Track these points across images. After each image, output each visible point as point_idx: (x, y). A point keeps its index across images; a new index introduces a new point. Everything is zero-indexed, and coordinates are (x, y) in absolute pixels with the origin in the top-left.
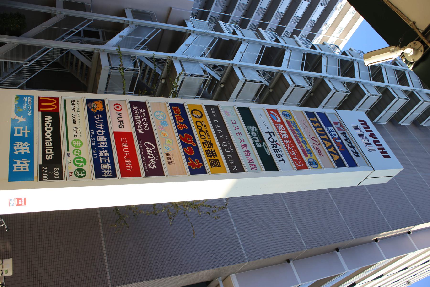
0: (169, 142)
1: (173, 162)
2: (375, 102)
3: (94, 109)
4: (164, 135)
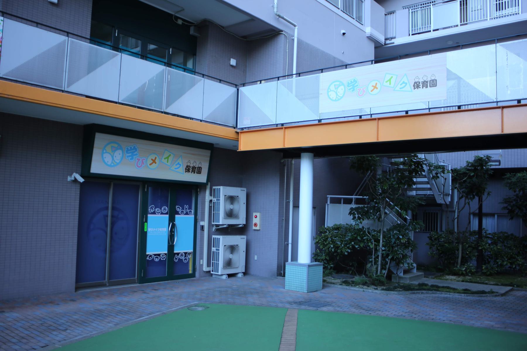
0: (390, 80)
1: (433, 78)
2: (346, 283)
3: (373, 218)
4: (375, 87)
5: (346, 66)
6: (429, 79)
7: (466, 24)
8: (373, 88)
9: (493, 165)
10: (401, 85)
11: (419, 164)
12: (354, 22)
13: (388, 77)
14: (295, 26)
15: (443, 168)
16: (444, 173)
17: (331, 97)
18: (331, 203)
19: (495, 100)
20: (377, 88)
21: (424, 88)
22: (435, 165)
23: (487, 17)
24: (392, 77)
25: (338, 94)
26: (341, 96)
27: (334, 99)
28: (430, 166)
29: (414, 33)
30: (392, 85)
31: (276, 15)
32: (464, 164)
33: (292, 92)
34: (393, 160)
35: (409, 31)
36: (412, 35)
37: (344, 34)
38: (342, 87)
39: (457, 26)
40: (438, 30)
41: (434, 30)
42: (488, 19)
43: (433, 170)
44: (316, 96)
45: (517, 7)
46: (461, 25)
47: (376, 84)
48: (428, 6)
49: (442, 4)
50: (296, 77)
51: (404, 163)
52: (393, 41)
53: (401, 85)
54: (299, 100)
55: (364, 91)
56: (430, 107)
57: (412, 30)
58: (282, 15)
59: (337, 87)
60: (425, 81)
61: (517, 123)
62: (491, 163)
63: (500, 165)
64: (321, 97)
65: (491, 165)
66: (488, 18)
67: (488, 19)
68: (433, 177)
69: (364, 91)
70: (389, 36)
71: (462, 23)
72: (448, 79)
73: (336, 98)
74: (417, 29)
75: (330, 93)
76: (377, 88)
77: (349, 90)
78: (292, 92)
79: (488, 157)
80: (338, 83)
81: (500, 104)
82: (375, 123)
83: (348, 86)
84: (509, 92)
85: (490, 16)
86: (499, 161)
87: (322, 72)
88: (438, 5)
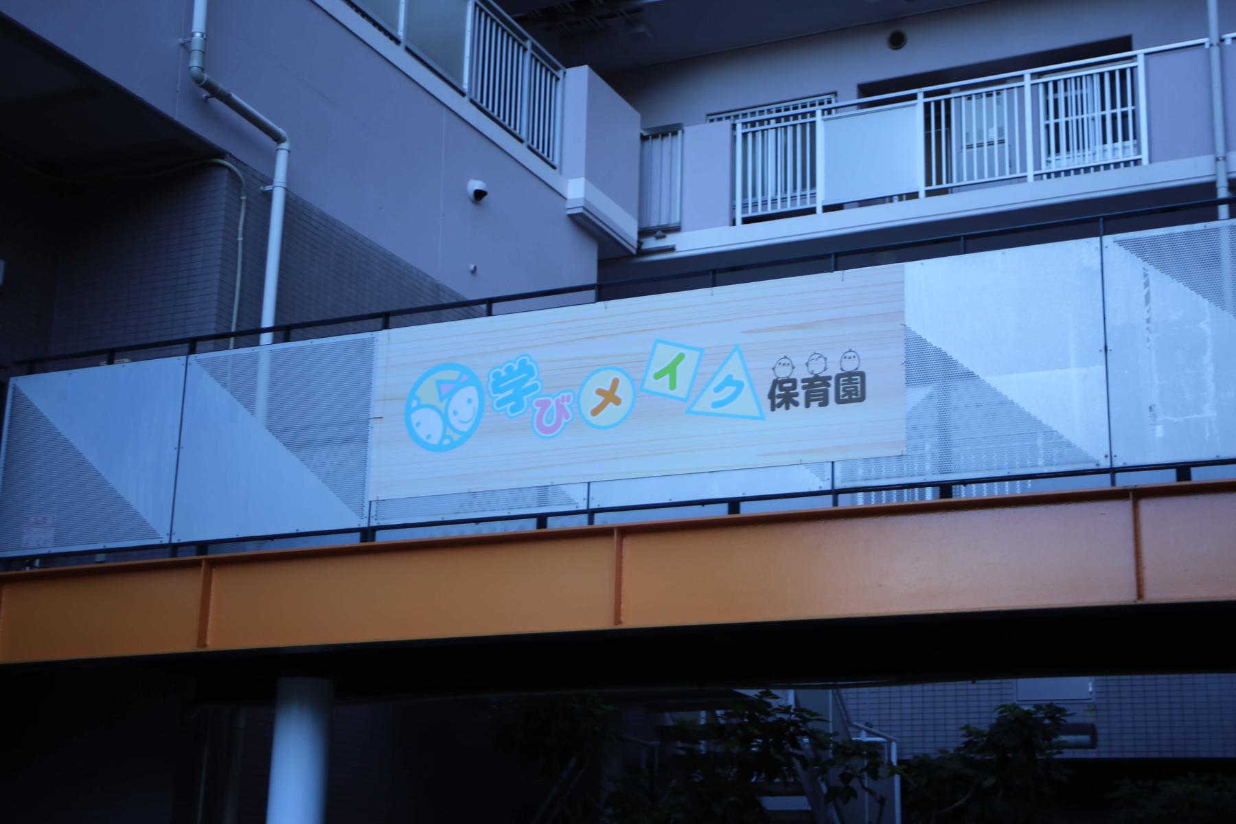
1: (850, 366)
5: (488, 306)
6: (833, 371)
7: (945, 191)
8: (601, 399)
9: (1070, 747)
10: (717, 390)
11: (782, 733)
12: (520, 151)
13: (664, 356)
14: (278, 139)
15: (874, 753)
16: (875, 776)
17: (422, 433)
18: (951, 496)
19: (1105, 464)
20: (617, 402)
21: (814, 405)
22: (838, 739)
23: (1024, 169)
24: (681, 356)
25: (454, 421)
26: (465, 428)
27: (434, 441)
28: (819, 742)
29: (750, 214)
30: (681, 390)
31: (198, 81)
32: (953, 740)
33: (251, 408)
34: (669, 719)
35: (733, 208)
36: (746, 221)
37: (479, 195)
38: (470, 392)
39: (913, 196)
40: (839, 207)
41: (827, 209)
42: (1030, 178)
43: (831, 763)
44: (355, 433)
45: (1131, 142)
46: (929, 194)
47: (615, 383)
48: (804, 115)
49: (855, 111)
50: (275, 341)
51: (715, 731)
52: (670, 240)
53: (717, 390)
54: (291, 446)
55: (562, 411)
56: (838, 485)
57: (745, 206)
58: (222, 86)
59: (447, 391)
60: (817, 377)
61: (1190, 560)
62: (1063, 738)
63: (1093, 745)
64: (376, 431)
65: (1063, 746)
66: (1030, 173)
67: (1030, 178)
68: (833, 792)
69: (562, 411)
70: (654, 223)
71: (934, 186)
72: (913, 380)
73: (444, 436)
74: (765, 203)
75: (415, 417)
76: (617, 402)
77: (500, 404)
78: (251, 408)
79: (1054, 711)
80: (452, 375)
81: (1123, 481)
82: (603, 551)
83: (497, 390)
84: (1159, 431)
85: (1037, 165)
86: (1090, 730)
87: (386, 326)
88: (842, 113)
